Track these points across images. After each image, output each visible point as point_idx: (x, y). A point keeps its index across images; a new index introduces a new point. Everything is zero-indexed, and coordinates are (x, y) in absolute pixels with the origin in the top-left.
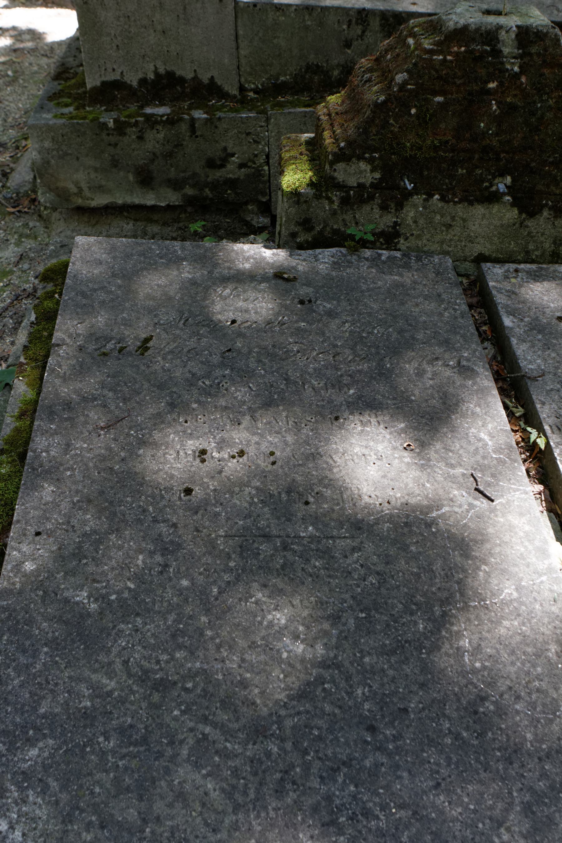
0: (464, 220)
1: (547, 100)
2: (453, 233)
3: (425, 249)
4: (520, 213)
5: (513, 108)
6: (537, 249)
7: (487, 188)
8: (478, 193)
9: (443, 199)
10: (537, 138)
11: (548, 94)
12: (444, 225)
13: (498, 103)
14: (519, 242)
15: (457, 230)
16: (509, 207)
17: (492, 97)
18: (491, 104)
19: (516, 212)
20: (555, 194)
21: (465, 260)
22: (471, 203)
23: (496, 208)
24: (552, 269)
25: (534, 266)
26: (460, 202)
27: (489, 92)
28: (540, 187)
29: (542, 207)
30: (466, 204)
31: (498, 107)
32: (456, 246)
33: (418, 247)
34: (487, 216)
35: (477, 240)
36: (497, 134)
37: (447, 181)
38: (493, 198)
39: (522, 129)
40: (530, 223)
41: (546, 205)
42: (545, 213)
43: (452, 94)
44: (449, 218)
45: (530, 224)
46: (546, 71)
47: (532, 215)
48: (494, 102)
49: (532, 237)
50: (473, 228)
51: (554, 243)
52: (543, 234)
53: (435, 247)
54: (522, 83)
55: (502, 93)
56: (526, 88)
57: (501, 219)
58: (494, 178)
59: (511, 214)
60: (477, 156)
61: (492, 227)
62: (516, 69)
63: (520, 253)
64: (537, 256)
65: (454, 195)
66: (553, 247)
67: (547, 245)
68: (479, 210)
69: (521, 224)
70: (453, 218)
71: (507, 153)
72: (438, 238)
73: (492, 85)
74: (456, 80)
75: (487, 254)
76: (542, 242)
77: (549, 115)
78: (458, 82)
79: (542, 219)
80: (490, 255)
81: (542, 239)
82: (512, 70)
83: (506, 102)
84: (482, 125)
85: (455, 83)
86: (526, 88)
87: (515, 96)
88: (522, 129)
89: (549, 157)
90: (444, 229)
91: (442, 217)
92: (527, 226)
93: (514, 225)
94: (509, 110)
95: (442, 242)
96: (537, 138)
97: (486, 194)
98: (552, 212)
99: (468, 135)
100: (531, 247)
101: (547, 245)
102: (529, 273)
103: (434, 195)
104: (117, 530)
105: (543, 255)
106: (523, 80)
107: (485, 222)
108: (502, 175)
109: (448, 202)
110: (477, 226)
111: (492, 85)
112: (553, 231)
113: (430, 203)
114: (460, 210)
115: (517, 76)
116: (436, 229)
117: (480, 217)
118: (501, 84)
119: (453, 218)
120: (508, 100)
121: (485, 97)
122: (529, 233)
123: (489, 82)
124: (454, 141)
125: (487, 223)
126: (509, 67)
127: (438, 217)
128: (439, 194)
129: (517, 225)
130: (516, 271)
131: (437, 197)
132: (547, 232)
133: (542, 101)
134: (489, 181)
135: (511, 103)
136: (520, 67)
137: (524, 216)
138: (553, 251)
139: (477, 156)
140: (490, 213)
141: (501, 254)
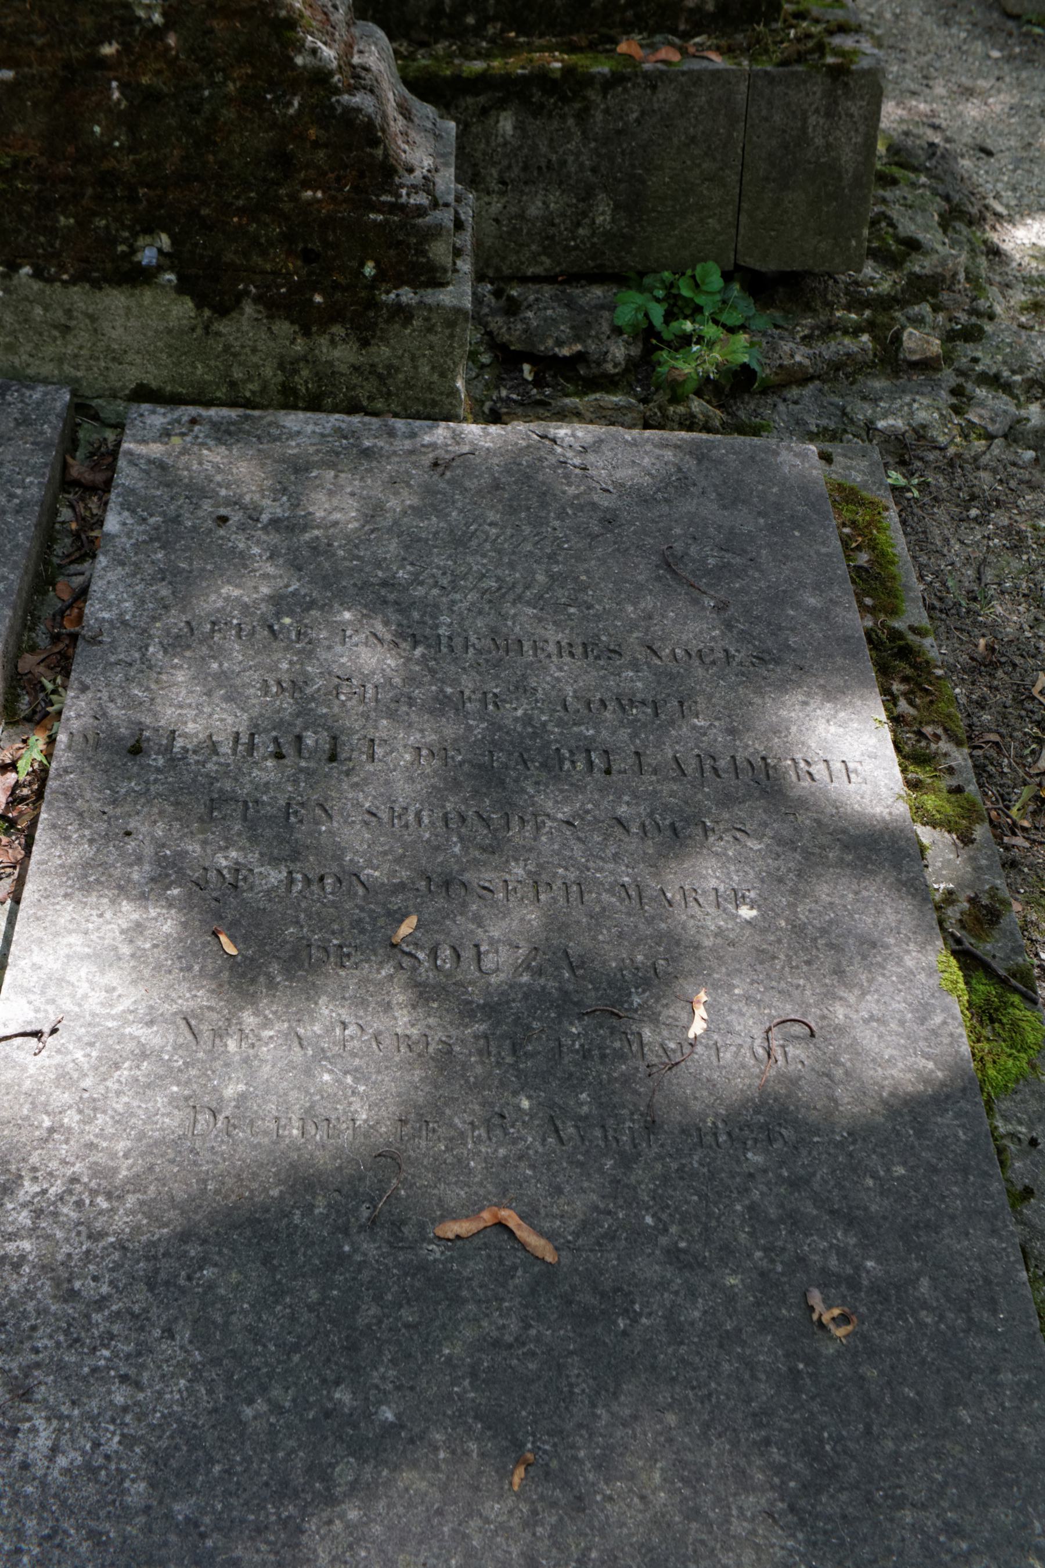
0: (93, 318)
1: (224, 83)
2: (77, 343)
3: (30, 371)
4: (199, 307)
5: (151, 98)
6: (250, 379)
7: (125, 256)
8: (109, 266)
9: (38, 274)
10: (211, 158)
11: (223, 70)
12: (55, 327)
13: (122, 87)
14: (212, 363)
15: (83, 337)
16: (174, 296)
17: (111, 74)
18: (110, 88)
19: (191, 304)
20: (263, 272)
21: (115, 397)
22: (96, 285)
23: (148, 296)
24: (269, 419)
25: (233, 413)
26: (74, 281)
27: (102, 63)
28: (229, 257)
29: (239, 297)
30: (87, 286)
31: (122, 93)
32: (89, 368)
33: (14, 367)
34: (135, 311)
35: (129, 357)
36: (132, 150)
37: (42, 239)
38: (139, 277)
39: (179, 139)
40: (222, 326)
41: (246, 292)
42: (249, 309)
43: (30, 66)
44: (60, 313)
45: (224, 331)
46: (217, 24)
47: (223, 311)
48: (114, 84)
49: (235, 355)
50: (114, 334)
51: (281, 366)
52: (254, 350)
53: (48, 369)
54: (168, 48)
55: (132, 65)
56: (177, 57)
57: (163, 316)
58: (135, 235)
59: (184, 309)
60: (90, 191)
61: (150, 334)
62: (157, 18)
63: (218, 385)
64: (253, 393)
65: (62, 268)
66: (280, 377)
67: (268, 372)
68: (116, 299)
69: (206, 329)
70: (69, 313)
71: (148, 186)
72: (50, 350)
73: (108, 50)
74: (34, 37)
75: (154, 385)
76: (257, 366)
77: (228, 114)
78: (40, 42)
79: (244, 320)
80: (160, 389)
81: (255, 359)
82: (150, 19)
83: (139, 84)
84: (97, 129)
85: (31, 43)
86: (177, 57)
87: (158, 72)
88: (179, 139)
89: (237, 197)
90: (56, 333)
91: (46, 309)
92: (218, 334)
93: (193, 329)
94: (146, 100)
95: (60, 360)
96: (211, 158)
97: (126, 266)
98: (261, 308)
99: (71, 149)
100: (238, 374)
101: (268, 372)
102: (215, 425)
103: (20, 266)
104: (807, 854)
105: (264, 389)
106: (171, 41)
107: (132, 322)
108: (149, 230)
109: (50, 280)
110: (121, 330)
111: (108, 50)
112: (272, 344)
113: (15, 282)
114: (78, 296)
115: (157, 33)
116: (41, 334)
117: (121, 312)
118: (126, 48)
119: (69, 313)
120: (145, 80)
121: (99, 74)
122: (227, 348)
123: (102, 43)
124: (43, 160)
125: (138, 324)
126: (141, 13)
127: (39, 311)
128: (32, 265)
129: (199, 331)
130: (193, 421)
131: (27, 270)
132: (261, 346)
133: (212, 84)
134: (125, 241)
135: (148, 86)
136: (164, 14)
137: (207, 313)
138: (283, 384)
139: (90, 191)
140: (140, 306)
141: (181, 385)
